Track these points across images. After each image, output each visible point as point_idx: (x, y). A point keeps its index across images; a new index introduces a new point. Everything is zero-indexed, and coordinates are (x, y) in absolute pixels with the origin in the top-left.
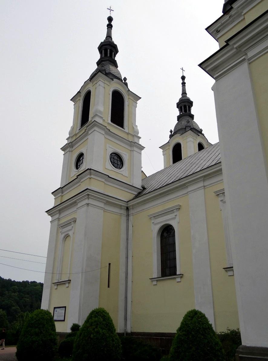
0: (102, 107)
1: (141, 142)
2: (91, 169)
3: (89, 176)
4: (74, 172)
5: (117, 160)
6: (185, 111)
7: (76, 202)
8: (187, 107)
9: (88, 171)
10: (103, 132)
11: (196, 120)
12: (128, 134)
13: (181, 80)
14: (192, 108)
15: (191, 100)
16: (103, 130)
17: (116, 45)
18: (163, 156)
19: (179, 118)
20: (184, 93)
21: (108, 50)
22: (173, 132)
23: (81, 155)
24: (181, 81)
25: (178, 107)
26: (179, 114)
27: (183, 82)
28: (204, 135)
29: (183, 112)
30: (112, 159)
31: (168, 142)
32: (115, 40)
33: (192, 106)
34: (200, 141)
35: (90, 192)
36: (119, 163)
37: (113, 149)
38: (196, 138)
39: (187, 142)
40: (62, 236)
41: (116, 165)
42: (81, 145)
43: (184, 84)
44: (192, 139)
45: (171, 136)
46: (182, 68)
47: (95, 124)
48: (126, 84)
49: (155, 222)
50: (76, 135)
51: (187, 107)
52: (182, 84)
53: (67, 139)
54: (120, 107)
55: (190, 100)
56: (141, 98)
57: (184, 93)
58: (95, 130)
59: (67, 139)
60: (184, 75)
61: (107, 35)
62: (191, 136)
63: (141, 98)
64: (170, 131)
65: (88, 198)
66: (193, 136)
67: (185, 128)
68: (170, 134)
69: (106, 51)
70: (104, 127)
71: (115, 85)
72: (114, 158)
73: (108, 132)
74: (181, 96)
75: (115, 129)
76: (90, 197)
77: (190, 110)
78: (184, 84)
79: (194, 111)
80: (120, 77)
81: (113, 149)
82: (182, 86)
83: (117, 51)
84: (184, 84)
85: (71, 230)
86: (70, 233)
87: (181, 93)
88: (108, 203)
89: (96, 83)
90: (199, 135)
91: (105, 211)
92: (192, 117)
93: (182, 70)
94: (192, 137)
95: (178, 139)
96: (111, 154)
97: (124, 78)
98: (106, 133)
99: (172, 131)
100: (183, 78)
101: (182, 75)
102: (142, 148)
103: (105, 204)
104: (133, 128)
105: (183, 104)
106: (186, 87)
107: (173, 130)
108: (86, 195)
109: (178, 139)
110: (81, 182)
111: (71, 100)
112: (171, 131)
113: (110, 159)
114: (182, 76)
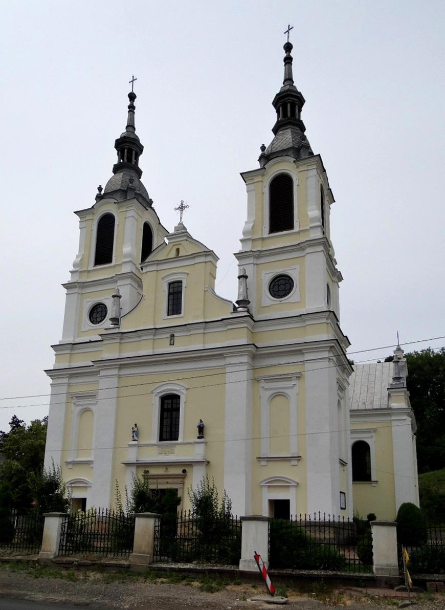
6: (129, 160)
8: (134, 152)
11: (143, 180)
13: (284, 51)
14: (141, 158)
15: (141, 142)
16: (75, 287)
17: (300, 93)
18: (79, 230)
19: (116, 169)
21: (129, 148)
22: (103, 192)
24: (284, 54)
25: (116, 147)
26: (116, 162)
27: (130, 104)
28: (154, 210)
29: (125, 161)
30: (99, 319)
31: (160, 224)
32: (300, 84)
33: (141, 153)
34: (147, 220)
36: (99, 309)
37: (149, 262)
39: (126, 218)
42: (322, 324)
43: (131, 109)
45: (99, 198)
46: (136, 79)
49: (77, 403)
51: (134, 152)
52: (129, 107)
55: (139, 142)
60: (290, 42)
61: (285, 77)
62: (135, 209)
64: (261, 148)
66: (137, 210)
68: (98, 192)
72: (102, 311)
76: (303, 352)
77: (137, 163)
81: (149, 262)
82: (129, 112)
87: (126, 125)
89: (126, 211)
90: (147, 210)
92: (139, 173)
93: (134, 82)
94: (136, 211)
95: (109, 207)
96: (92, 322)
99: (102, 189)
100: (288, 47)
101: (286, 42)
106: (136, 116)
107: (104, 187)
109: (109, 207)
112: (100, 189)
113: (99, 323)
114: (286, 44)
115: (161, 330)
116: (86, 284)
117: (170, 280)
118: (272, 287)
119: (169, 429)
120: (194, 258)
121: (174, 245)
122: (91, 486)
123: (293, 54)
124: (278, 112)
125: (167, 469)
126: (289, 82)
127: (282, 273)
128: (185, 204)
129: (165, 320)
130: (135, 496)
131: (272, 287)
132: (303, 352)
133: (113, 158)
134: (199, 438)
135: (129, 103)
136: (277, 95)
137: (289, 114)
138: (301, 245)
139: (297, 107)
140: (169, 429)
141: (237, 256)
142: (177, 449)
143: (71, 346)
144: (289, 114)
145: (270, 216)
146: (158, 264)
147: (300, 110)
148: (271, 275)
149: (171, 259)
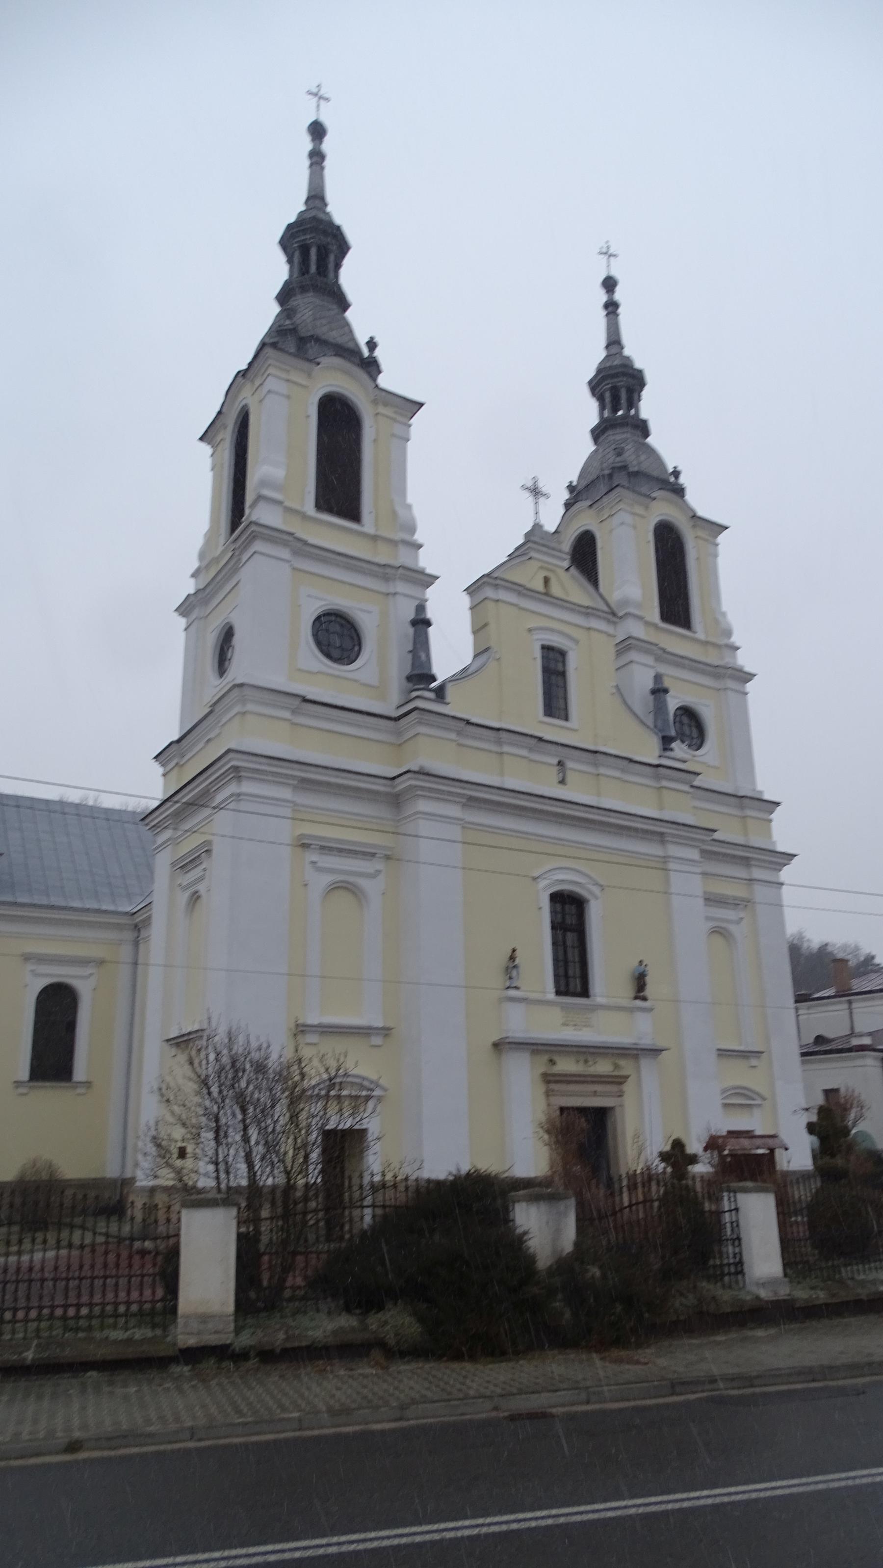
0: (286, 461)
1: (744, 660)
2: (241, 685)
3: (237, 709)
4: (214, 686)
5: (337, 636)
7: (209, 790)
9: (236, 692)
10: (285, 554)
12: (706, 643)
16: (285, 544)
17: (338, 228)
19: (597, 434)
20: (614, 342)
21: (618, 386)
23: (228, 635)
32: (339, 211)
35: (238, 760)
38: (647, 508)
40: (183, 898)
41: (336, 653)
43: (610, 309)
44: (628, 518)
47: (253, 532)
48: (679, 491)
49: (185, 883)
50: (216, 560)
53: (193, 575)
54: (344, 457)
56: (421, 405)
57: (614, 342)
58: (255, 553)
59: (193, 576)
61: (309, 191)
63: (421, 405)
65: (239, 778)
67: (610, 476)
69: (305, 250)
70: (286, 537)
71: (333, 378)
72: (327, 630)
73: (303, 548)
74: (602, 354)
75: (331, 532)
76: (242, 774)
78: (612, 307)
79: (648, 407)
80: (351, 345)
82: (607, 315)
83: (343, 248)
84: (612, 307)
85: (201, 879)
86: (201, 888)
88: (305, 785)
91: (465, 826)
92: (642, 428)
95: (586, 521)
96: (318, 618)
97: (367, 340)
98: (296, 553)
102: (748, 677)
103: (295, 788)
104: (394, 513)
105: (607, 385)
108: (229, 769)
110: (220, 724)
111: (201, 439)
112: (571, 488)
115: (549, 746)
116: (308, 549)
117: (549, 640)
118: (356, 648)
119: (572, 975)
120: (587, 615)
121: (541, 568)
122: (759, 1105)
123: (327, 146)
124: (290, 261)
125: (586, 1061)
126: (317, 203)
127: (345, 610)
128: (530, 484)
129: (531, 716)
130: (712, 1166)
131: (356, 648)
132: (242, 774)
133: (589, 412)
134: (636, 998)
135: (603, 298)
136: (290, 226)
137: (313, 268)
138: (388, 570)
139: (332, 258)
140: (572, 975)
141: (470, 591)
142: (785, 1136)
143: (297, 702)
144: (313, 268)
145: (317, 483)
146: (519, 594)
147: (338, 266)
148: (323, 603)
149: (507, 581)
